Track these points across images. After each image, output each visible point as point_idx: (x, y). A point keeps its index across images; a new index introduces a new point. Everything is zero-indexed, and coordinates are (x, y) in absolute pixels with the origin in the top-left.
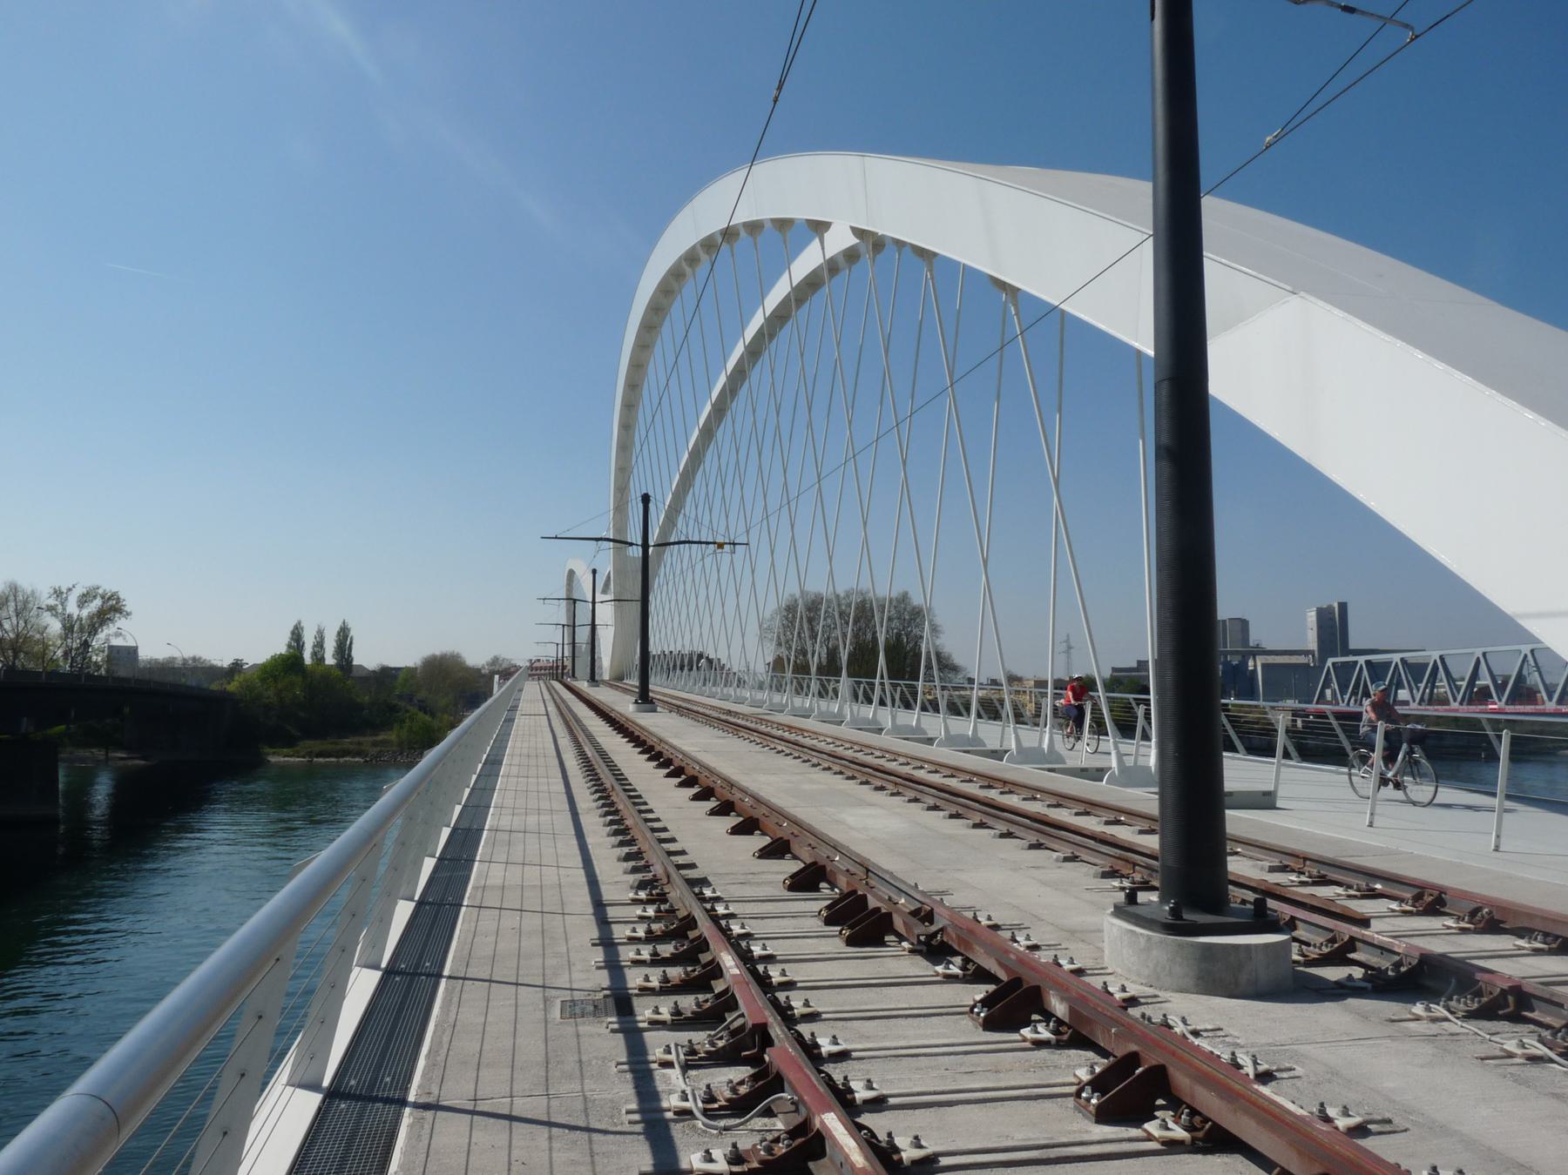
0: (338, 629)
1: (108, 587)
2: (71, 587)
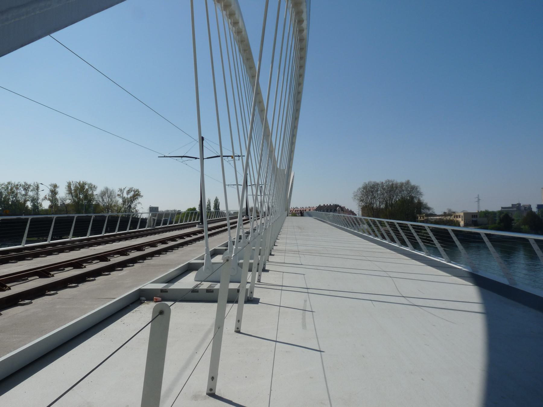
0: (215, 199)
1: (135, 187)
2: (124, 188)
